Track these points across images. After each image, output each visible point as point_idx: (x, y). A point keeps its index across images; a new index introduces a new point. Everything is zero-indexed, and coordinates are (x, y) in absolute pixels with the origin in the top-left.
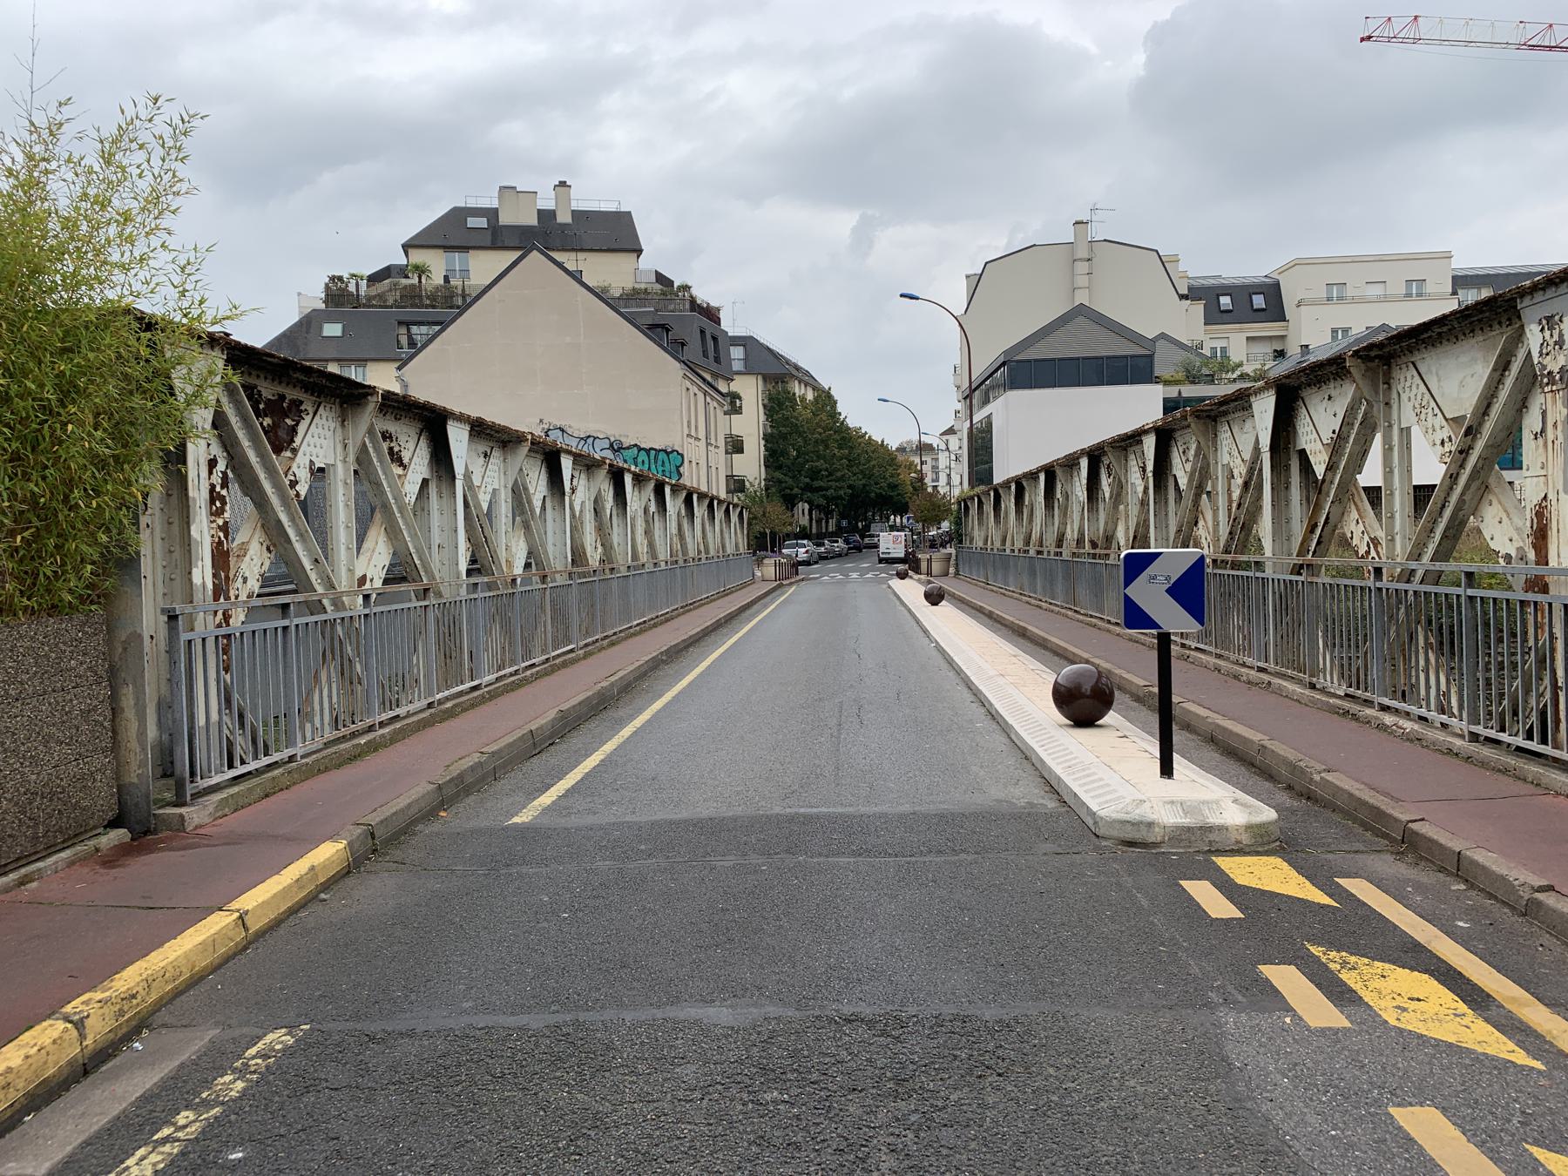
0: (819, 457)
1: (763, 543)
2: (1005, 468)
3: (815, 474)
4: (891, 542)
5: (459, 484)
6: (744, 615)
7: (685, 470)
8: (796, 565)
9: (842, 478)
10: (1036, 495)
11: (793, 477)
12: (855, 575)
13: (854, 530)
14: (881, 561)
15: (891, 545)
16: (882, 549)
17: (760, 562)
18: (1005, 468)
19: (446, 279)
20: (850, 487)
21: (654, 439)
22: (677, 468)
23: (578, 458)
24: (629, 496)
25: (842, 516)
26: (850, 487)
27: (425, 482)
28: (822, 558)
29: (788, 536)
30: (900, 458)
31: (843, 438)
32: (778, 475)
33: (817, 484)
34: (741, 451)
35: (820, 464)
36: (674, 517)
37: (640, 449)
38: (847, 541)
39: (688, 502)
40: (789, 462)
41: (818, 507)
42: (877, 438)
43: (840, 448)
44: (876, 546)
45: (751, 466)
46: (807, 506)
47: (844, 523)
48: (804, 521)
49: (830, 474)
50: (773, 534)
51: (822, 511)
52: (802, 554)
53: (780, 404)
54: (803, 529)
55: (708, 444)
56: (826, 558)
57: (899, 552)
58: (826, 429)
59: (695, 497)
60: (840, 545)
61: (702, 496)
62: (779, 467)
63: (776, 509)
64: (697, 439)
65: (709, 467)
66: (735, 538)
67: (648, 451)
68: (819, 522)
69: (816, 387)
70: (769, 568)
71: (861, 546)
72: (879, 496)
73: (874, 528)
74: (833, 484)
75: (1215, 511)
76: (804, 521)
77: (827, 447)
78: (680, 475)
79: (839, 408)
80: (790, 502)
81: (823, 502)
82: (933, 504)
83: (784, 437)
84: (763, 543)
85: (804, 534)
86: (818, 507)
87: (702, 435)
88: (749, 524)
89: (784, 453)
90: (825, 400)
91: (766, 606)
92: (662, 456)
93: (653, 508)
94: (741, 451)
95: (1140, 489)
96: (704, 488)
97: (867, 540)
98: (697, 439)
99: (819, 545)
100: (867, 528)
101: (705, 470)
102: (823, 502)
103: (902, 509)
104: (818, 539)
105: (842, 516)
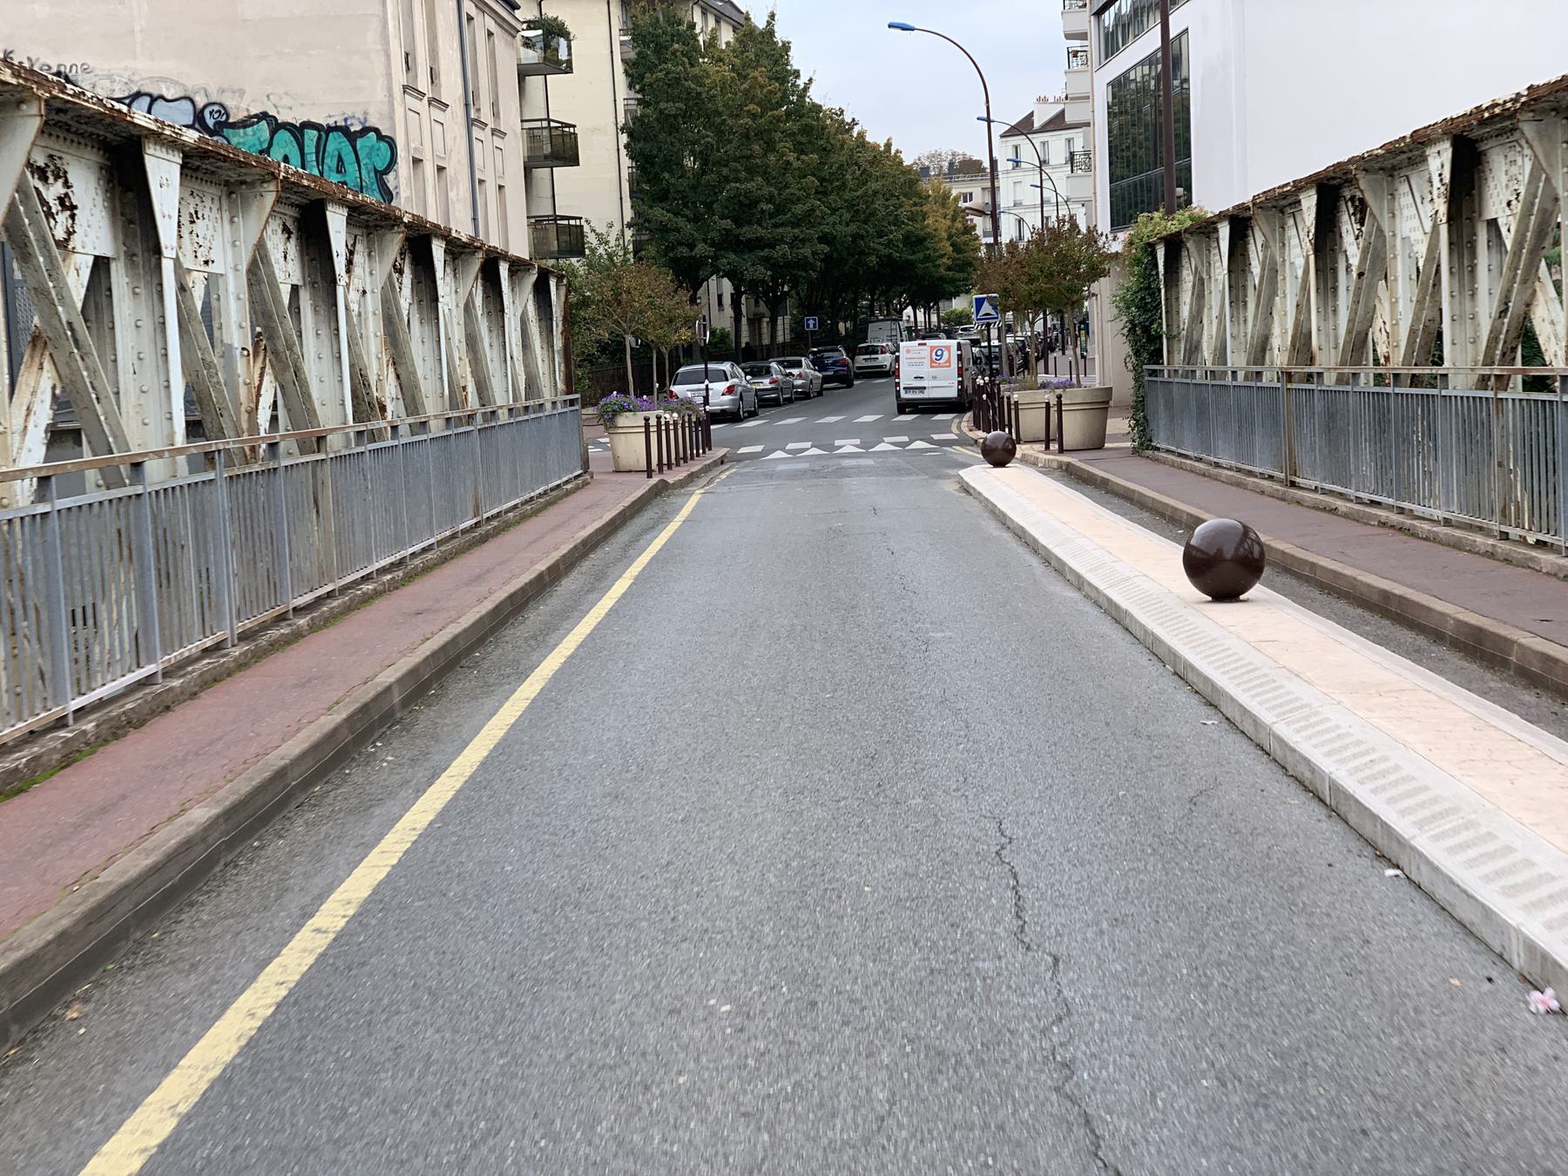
0: (752, 172)
1: (613, 365)
2: (1216, 186)
3: (744, 210)
4: (927, 365)
5: (168, 266)
6: (494, 654)
7: (401, 178)
8: (705, 422)
9: (807, 219)
10: (1416, 217)
11: (696, 219)
12: (849, 446)
13: (829, 338)
14: (904, 407)
15: (925, 370)
16: (905, 379)
17: (608, 421)
18: (1228, 168)
19: (676, 291)
20: (824, 239)
21: (320, 105)
22: (380, 175)
23: (197, 166)
24: (439, 282)
25: (807, 308)
26: (824, 239)
27: (101, 266)
28: (767, 403)
29: (689, 352)
30: (926, 186)
31: (807, 130)
32: (659, 213)
33: (748, 232)
34: (573, 160)
35: (754, 185)
36: (458, 316)
37: (276, 126)
38: (819, 363)
39: (489, 275)
40: (683, 184)
41: (753, 287)
42: (875, 137)
43: (800, 149)
44: (894, 373)
45: (597, 191)
46: (727, 286)
47: (811, 323)
48: (723, 320)
49: (780, 210)
50: (642, 354)
51: (759, 293)
52: (719, 395)
53: (660, 49)
54: (720, 338)
55: (471, 123)
56: (775, 403)
57: (945, 386)
58: (768, 104)
59: (504, 269)
60: (805, 372)
61: (458, 251)
62: (662, 197)
63: (654, 287)
64: (435, 102)
65: (476, 184)
66: (520, 356)
67: (298, 131)
68: (755, 321)
69: (742, 24)
70: (630, 439)
71: (849, 374)
72: (887, 262)
73: (878, 334)
74: (789, 232)
75: (1394, 304)
76: (723, 320)
77: (770, 146)
78: (388, 195)
79: (796, 60)
80: (690, 275)
81: (763, 273)
82: (1062, 258)
83: (669, 123)
84: (613, 365)
85: (719, 349)
86: (753, 287)
87: (451, 90)
88: (569, 320)
89: (673, 163)
90: (763, 50)
91: (599, 584)
92: (336, 143)
93: (405, 297)
94: (573, 160)
95: (1422, 249)
96: (462, 229)
97: (861, 360)
98: (435, 102)
99: (756, 373)
100: (860, 333)
101: (458, 178)
102: (763, 273)
103: (930, 292)
104: (751, 358)
105: (807, 308)
